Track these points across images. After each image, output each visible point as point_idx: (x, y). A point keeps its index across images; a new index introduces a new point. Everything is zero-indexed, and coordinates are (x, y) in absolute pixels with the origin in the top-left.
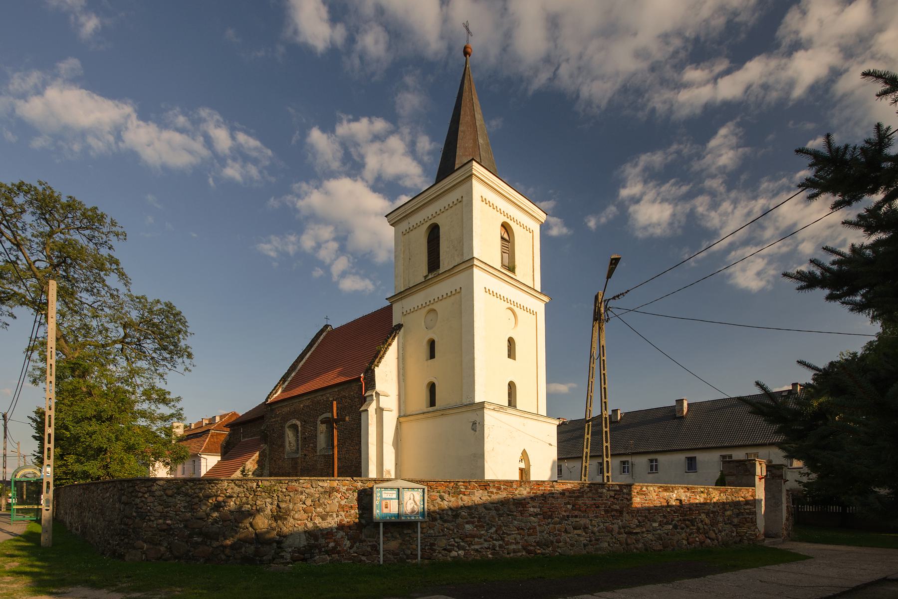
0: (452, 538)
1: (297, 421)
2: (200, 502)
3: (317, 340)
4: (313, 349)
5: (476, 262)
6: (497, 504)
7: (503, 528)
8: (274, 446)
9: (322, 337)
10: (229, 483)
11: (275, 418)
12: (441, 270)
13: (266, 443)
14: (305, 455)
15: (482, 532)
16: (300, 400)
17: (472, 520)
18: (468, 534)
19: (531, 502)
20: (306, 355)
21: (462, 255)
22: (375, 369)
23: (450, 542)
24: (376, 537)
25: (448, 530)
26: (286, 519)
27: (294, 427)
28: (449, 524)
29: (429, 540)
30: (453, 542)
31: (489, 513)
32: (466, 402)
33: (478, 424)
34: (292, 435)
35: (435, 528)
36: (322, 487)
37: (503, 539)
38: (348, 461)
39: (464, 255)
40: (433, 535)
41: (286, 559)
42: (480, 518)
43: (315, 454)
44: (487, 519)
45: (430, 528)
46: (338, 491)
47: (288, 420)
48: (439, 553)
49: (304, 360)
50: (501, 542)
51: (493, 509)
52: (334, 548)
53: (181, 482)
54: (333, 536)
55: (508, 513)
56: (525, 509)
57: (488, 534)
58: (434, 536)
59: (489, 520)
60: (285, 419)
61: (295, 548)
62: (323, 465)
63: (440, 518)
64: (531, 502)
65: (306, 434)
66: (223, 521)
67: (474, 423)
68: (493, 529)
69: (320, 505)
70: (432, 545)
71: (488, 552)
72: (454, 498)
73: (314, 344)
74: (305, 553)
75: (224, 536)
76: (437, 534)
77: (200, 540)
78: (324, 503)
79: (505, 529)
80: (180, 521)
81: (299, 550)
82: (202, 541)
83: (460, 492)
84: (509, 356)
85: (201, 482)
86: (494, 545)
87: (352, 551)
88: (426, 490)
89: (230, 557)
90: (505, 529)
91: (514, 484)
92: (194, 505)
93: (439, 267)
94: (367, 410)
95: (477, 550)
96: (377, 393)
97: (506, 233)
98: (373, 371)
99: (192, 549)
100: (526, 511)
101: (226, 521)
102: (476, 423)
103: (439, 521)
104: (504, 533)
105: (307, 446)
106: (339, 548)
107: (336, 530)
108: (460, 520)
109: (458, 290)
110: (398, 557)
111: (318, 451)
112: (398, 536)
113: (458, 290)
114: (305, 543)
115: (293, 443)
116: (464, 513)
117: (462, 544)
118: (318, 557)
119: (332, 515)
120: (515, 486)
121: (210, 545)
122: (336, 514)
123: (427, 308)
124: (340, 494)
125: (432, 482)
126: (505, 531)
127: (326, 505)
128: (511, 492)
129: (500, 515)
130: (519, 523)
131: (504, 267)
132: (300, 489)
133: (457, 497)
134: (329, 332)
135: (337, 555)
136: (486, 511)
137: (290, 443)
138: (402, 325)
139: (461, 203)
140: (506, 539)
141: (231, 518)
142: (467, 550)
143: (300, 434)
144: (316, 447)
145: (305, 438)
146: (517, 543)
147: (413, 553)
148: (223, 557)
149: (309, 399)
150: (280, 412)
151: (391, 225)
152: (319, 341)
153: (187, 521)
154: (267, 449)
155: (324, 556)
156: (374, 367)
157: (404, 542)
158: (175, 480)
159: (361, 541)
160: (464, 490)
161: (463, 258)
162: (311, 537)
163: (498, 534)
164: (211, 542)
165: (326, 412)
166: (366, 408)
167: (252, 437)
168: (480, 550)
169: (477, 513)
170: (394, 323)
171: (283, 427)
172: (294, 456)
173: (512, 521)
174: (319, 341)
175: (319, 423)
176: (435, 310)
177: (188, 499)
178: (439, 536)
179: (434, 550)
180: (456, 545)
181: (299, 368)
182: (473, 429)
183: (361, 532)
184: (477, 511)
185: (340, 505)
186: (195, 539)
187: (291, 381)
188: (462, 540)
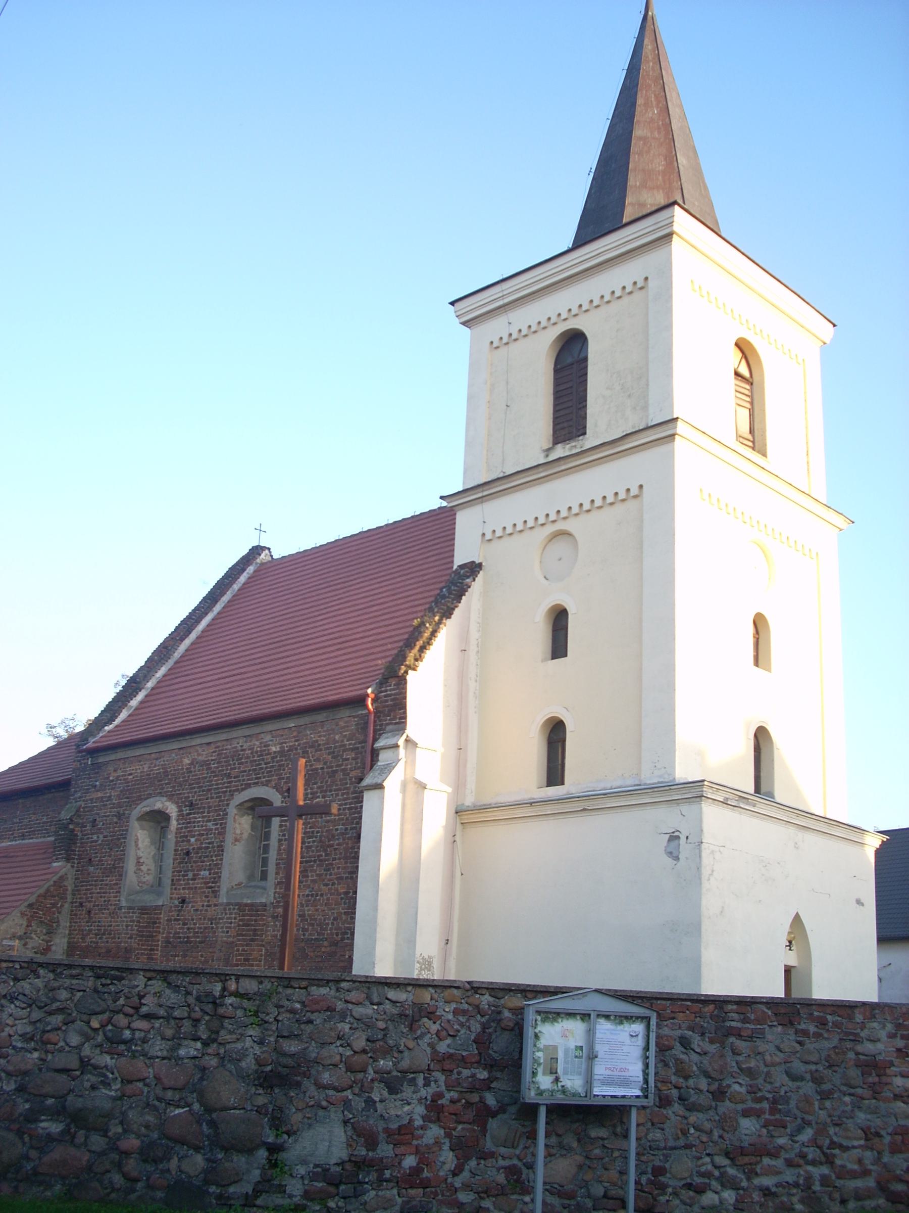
0: (708, 1155)
1: (168, 804)
2: (66, 1024)
3: (230, 585)
4: (218, 608)
5: (680, 427)
6: (816, 1064)
7: (832, 1131)
8: (91, 869)
9: (243, 578)
10: (150, 979)
11: (102, 788)
12: (590, 440)
13: (68, 859)
14: (183, 901)
15: (781, 1141)
16: (184, 744)
17: (758, 1106)
18: (746, 1144)
19: (896, 1062)
20: (198, 621)
21: (645, 408)
22: (408, 678)
23: (703, 1165)
24: (521, 1146)
25: (698, 1133)
26: (298, 1084)
27: (159, 819)
28: (700, 1115)
29: (652, 1158)
30: (710, 1167)
31: (799, 1088)
32: (649, 777)
33: (683, 839)
34: (147, 841)
35: (665, 1126)
36: (394, 1002)
37: (829, 1161)
38: (313, 925)
39: (651, 410)
40: (662, 1145)
41: (291, 1196)
42: (775, 1102)
43: (213, 901)
44: (793, 1104)
45: (653, 1124)
46: (431, 1015)
47: (141, 799)
48: (675, 1194)
49: (193, 636)
50: (825, 1170)
51: (808, 1076)
52: (416, 1171)
53: (21, 968)
54: (414, 1137)
55: (844, 1088)
56: (884, 1079)
57: (797, 1145)
58: (665, 1148)
59: (798, 1108)
60: (133, 795)
61: (316, 1166)
62: (232, 932)
63: (680, 1098)
64: (896, 1062)
65: (193, 840)
66: (122, 1081)
67: (674, 838)
68: (807, 1135)
69: (387, 1051)
70: (659, 1171)
71: (793, 1195)
72: (714, 1046)
73: (223, 594)
74: (341, 1182)
75: (121, 1123)
76: (671, 1143)
77: (55, 1128)
78: (397, 1046)
79: (836, 1134)
80: (9, 1074)
81: (323, 1173)
82: (62, 1133)
83: (732, 1032)
84: (757, 663)
85: (74, 972)
86: (809, 1178)
87: (458, 1182)
88: (653, 1022)
89: (136, 1180)
90: (836, 1134)
91: (857, 1011)
92: (48, 1031)
93: (582, 431)
94: (380, 787)
95: (768, 1189)
96: (407, 741)
97: (744, 361)
98: (402, 682)
99: (33, 1154)
100: (886, 1084)
101: (130, 1082)
102: (678, 837)
103: (676, 1105)
104: (833, 1145)
105: (190, 875)
106: (426, 1174)
107: (421, 1123)
108: (726, 1106)
109: (634, 491)
110: (573, 1202)
111: (223, 891)
112: (575, 1144)
113: (634, 491)
114: (344, 1155)
115: (149, 864)
116: (736, 1087)
117: (731, 1171)
118: (373, 1193)
119: (414, 1079)
120: (859, 1018)
121: (85, 1144)
122: (425, 1078)
123: (550, 529)
124: (438, 1022)
125: (664, 1002)
126: (835, 1139)
127: (401, 1052)
128: (851, 1034)
129: (825, 1096)
130: (869, 1117)
131: (741, 440)
132: (340, 1005)
133: (722, 1044)
134: (262, 564)
135: (421, 1190)
136: (790, 1083)
137: (139, 863)
138: (480, 566)
139: (643, 291)
140: (838, 1162)
141: (146, 1075)
142: (743, 1189)
143: (171, 836)
144: (217, 878)
145: (188, 853)
146: (866, 1173)
147: (612, 1193)
148: (117, 1179)
149: (209, 743)
150: (120, 773)
151: (457, 316)
152: (236, 587)
153: (26, 1073)
154: (69, 876)
155: (388, 1192)
156: (406, 672)
157: (587, 1162)
158: (5, 961)
159: (485, 1156)
160: (739, 1025)
161: (647, 416)
162: (358, 1136)
163: (818, 1147)
164: (87, 1137)
165: (257, 783)
166: (379, 781)
167: (23, 837)
168: (774, 1189)
169: (768, 1087)
170: (459, 559)
171: (122, 817)
172: (149, 900)
173: (852, 1111)
174: (236, 587)
175: (232, 811)
176: (569, 534)
177: (36, 1015)
178: (675, 1148)
179: (663, 1187)
180: (717, 1173)
181: (177, 655)
182: (670, 854)
183: (484, 1131)
184: (771, 1083)
185: (435, 1052)
186: (43, 1125)
187: (153, 689)
188: (732, 1159)
